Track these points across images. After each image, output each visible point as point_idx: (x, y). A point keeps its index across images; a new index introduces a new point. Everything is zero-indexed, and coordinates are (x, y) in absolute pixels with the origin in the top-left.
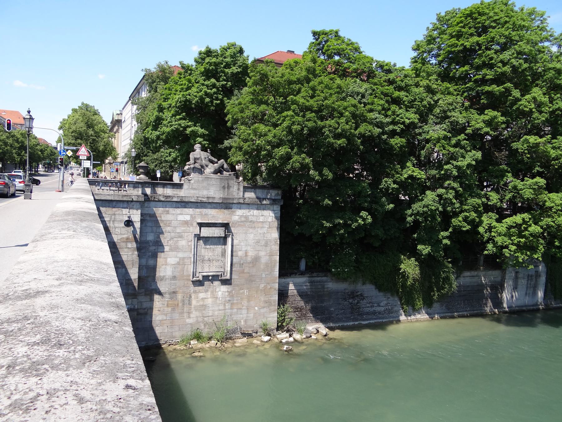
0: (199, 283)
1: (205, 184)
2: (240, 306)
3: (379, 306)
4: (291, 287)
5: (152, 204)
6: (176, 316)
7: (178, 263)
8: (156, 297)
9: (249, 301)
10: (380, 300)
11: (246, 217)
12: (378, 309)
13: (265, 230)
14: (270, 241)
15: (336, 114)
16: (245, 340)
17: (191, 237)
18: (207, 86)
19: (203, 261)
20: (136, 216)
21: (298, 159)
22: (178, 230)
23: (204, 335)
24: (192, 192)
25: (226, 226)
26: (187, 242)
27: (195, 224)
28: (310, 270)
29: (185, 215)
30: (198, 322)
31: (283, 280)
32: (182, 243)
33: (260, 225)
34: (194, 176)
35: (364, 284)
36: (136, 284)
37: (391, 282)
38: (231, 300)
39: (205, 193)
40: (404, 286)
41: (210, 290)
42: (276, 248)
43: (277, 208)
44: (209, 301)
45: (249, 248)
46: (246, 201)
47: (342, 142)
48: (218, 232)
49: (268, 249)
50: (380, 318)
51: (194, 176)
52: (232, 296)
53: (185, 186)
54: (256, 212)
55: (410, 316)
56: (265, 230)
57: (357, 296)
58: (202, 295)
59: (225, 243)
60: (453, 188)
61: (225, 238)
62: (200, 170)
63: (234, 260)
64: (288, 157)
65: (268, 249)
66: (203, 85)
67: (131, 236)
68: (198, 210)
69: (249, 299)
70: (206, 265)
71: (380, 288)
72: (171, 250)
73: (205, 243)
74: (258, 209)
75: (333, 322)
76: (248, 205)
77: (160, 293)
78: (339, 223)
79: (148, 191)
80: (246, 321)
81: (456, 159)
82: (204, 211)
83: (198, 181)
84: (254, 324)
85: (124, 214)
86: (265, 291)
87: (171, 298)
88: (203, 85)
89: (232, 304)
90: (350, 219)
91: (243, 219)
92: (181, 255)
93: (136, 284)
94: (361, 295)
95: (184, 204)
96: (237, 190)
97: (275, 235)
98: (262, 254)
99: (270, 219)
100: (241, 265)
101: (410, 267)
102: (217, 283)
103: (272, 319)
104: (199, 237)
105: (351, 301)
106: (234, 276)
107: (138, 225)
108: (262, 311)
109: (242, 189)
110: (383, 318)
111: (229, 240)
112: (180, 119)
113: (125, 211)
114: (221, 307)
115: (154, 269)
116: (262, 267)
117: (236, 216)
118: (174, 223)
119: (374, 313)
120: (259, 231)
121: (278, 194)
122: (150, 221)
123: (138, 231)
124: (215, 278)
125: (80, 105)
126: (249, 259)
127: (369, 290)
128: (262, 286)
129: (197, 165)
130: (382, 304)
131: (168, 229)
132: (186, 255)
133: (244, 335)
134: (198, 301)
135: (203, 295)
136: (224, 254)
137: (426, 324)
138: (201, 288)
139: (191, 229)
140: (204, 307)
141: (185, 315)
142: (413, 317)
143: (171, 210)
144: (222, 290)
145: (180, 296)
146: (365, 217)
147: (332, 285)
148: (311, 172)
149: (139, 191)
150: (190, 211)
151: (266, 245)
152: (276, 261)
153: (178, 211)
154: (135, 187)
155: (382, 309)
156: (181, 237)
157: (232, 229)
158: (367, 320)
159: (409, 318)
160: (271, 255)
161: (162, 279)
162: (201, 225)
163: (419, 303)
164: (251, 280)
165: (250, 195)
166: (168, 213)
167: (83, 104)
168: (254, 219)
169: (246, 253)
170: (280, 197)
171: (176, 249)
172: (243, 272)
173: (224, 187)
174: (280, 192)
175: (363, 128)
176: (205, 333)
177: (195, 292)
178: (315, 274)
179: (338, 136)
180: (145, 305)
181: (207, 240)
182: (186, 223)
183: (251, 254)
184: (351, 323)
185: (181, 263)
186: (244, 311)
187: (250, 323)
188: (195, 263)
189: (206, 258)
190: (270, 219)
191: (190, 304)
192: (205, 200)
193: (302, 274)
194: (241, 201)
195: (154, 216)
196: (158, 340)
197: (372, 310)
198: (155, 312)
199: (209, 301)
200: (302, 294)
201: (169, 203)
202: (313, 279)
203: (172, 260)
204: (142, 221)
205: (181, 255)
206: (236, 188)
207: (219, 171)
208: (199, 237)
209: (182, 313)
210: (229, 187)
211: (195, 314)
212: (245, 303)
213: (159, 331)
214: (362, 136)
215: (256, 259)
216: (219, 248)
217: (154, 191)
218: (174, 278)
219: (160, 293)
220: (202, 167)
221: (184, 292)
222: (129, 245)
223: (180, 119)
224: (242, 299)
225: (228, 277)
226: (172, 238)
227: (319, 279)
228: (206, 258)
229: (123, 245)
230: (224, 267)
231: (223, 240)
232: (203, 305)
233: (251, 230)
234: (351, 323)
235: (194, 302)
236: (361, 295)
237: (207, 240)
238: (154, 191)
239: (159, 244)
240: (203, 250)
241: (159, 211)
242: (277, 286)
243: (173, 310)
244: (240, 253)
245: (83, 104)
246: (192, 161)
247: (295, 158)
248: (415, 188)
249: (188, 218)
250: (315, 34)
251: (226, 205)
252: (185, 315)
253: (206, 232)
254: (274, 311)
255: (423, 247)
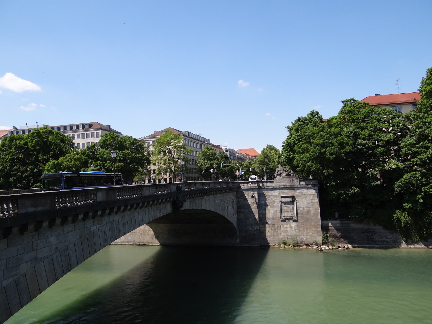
0: (284, 221)
1: (282, 180)
2: (303, 232)
3: (386, 238)
4: (330, 225)
5: (263, 189)
6: (275, 234)
7: (274, 213)
8: (267, 225)
9: (307, 230)
10: (389, 236)
11: (302, 193)
12: (386, 240)
13: (311, 198)
14: (315, 203)
15: (331, 145)
16: (305, 247)
17: (279, 202)
18: (297, 136)
19: (284, 212)
20: (256, 194)
21: (316, 166)
22: (273, 199)
23: (287, 243)
24: (278, 184)
25: (293, 197)
26: (277, 204)
27: (280, 197)
28: (341, 217)
29: (275, 193)
30: (284, 237)
31: (325, 222)
32: (275, 204)
33: (309, 196)
34: (278, 178)
35: (375, 225)
36: (258, 220)
37: (391, 225)
38: (298, 229)
39: (283, 184)
40: (400, 227)
41: (289, 224)
42: (318, 206)
43: (317, 188)
44: (289, 229)
45: (305, 206)
46: (301, 186)
47: (333, 157)
48: (290, 200)
49: (314, 207)
50: (387, 245)
51: (278, 178)
52: (299, 227)
53: (275, 182)
54: (306, 190)
55: (410, 245)
56: (311, 198)
57: (371, 232)
58: (285, 226)
59: (293, 204)
60: (419, 171)
61: (293, 202)
62: (280, 175)
63: (298, 212)
64: (312, 165)
65: (314, 207)
66: (296, 136)
67: (255, 202)
68: (281, 191)
69: (307, 229)
70: (286, 213)
71: (385, 227)
72: (271, 207)
73: (285, 204)
74: (307, 189)
75: (356, 244)
76: (303, 188)
77: (268, 224)
78: (341, 193)
79: (261, 185)
80: (306, 239)
81: (420, 155)
82: (283, 191)
83: (279, 180)
84: (311, 241)
85: (252, 193)
86: (314, 226)
87: (273, 227)
88: (296, 136)
89: (299, 231)
90: (348, 190)
91: (301, 194)
92: (275, 209)
93: (258, 220)
94: (374, 231)
95: (274, 189)
96: (296, 182)
97: (317, 200)
98: (311, 209)
99: (313, 193)
100: (302, 214)
101: (403, 217)
102: (291, 221)
103: (320, 239)
104: (282, 202)
105: (367, 234)
106: (298, 219)
107: (257, 198)
108: (314, 235)
109: (299, 181)
110: (390, 245)
111: (295, 203)
112: (288, 152)
113: (252, 192)
114: (294, 232)
115: (264, 215)
116: (312, 215)
117: (298, 192)
118: (271, 197)
119: (383, 241)
120: (308, 200)
121: (316, 182)
122: (262, 196)
123: (257, 200)
124: (290, 219)
125: (267, 146)
126: (305, 211)
127: (379, 229)
128: (313, 223)
129: (279, 173)
130: (389, 237)
131: (269, 199)
132: (277, 209)
133: (306, 245)
134: (284, 229)
135: (286, 226)
136: (293, 209)
137: (425, 250)
138: (284, 223)
139: (279, 199)
140: (287, 231)
141: (279, 234)
142: (412, 246)
143: (270, 191)
144: (294, 224)
145: (276, 226)
146: (354, 190)
147: (354, 225)
148: (325, 172)
149: (256, 185)
150: (277, 191)
151: (313, 205)
152: (318, 212)
153: (273, 191)
154: (255, 184)
155: (389, 240)
156: (275, 202)
157: (296, 198)
158: (378, 245)
159: (409, 246)
160: (316, 209)
161: (269, 219)
162: (282, 197)
163: (416, 238)
164: (307, 220)
165: (303, 183)
166: (269, 192)
167: (268, 145)
168: (306, 193)
169: (303, 208)
170: (317, 183)
171: (273, 207)
172: (303, 217)
173: (291, 181)
174: (317, 181)
175: (347, 149)
176: (288, 242)
177: (282, 225)
178: (343, 219)
179: (332, 154)
180: (263, 229)
181: (285, 203)
182: (276, 196)
183: (306, 209)
184: (368, 246)
185: (275, 212)
186: (305, 234)
187: (308, 240)
188: (281, 212)
189: (286, 211)
190: (313, 193)
191: (280, 229)
192: (283, 187)
193: (336, 219)
194: (299, 186)
195: (263, 194)
196: (269, 243)
197: (382, 240)
198: (266, 232)
199: (289, 229)
200: (336, 229)
201: (268, 189)
202: (343, 222)
203: (272, 211)
204: (258, 196)
205: (275, 209)
206: (296, 181)
207: (288, 175)
208: (282, 202)
209: (278, 233)
210: (293, 181)
211: (283, 234)
212: (305, 230)
213: (269, 239)
214: (346, 153)
215: (309, 211)
216: (291, 206)
217: (263, 185)
218: (273, 218)
219: (268, 224)
220: (281, 173)
221: (277, 224)
222: (254, 205)
223: (288, 152)
224: (303, 229)
225: (296, 219)
226: (271, 203)
227: (346, 222)
228: (286, 211)
229: (252, 205)
230: (294, 214)
231: (292, 203)
232: (286, 230)
233: (305, 199)
234: (368, 246)
235: (282, 229)
236: (374, 231)
237: (285, 203)
238: (263, 185)
239: (266, 205)
240: (284, 207)
241: (265, 192)
242: (320, 224)
243: (274, 231)
244: (301, 209)
245: (268, 145)
246: (277, 172)
247: (314, 166)
248: (397, 173)
249: (277, 194)
250: (343, 102)
251: (292, 188)
252: (279, 234)
253: (284, 200)
254: (320, 235)
255: (406, 204)
